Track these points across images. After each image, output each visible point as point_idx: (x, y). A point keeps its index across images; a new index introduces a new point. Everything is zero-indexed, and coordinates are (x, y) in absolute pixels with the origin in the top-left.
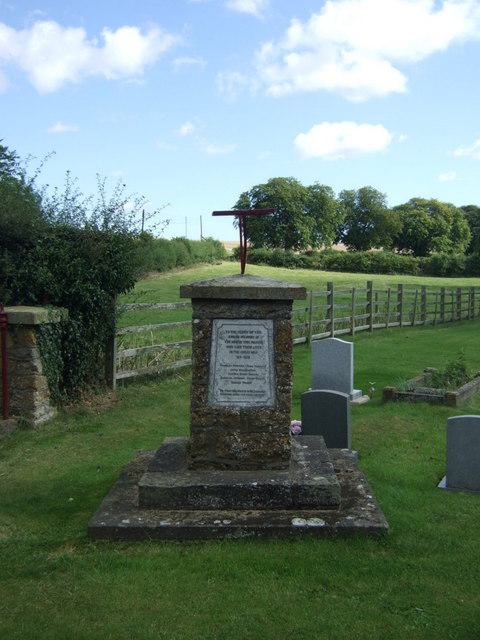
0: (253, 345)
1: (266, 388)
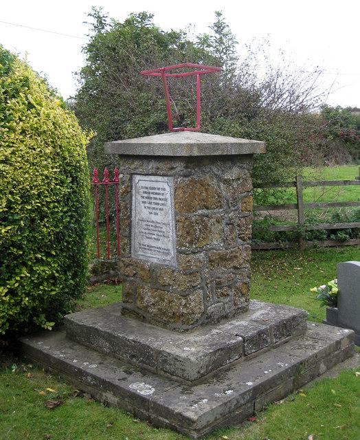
0: (160, 202)
1: (170, 246)
